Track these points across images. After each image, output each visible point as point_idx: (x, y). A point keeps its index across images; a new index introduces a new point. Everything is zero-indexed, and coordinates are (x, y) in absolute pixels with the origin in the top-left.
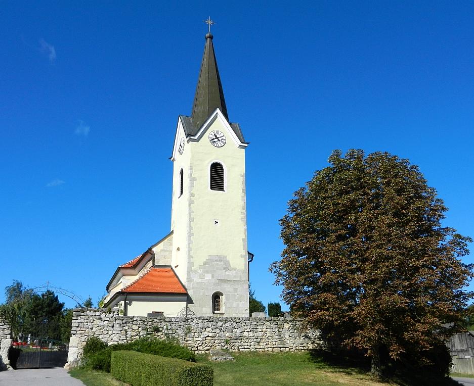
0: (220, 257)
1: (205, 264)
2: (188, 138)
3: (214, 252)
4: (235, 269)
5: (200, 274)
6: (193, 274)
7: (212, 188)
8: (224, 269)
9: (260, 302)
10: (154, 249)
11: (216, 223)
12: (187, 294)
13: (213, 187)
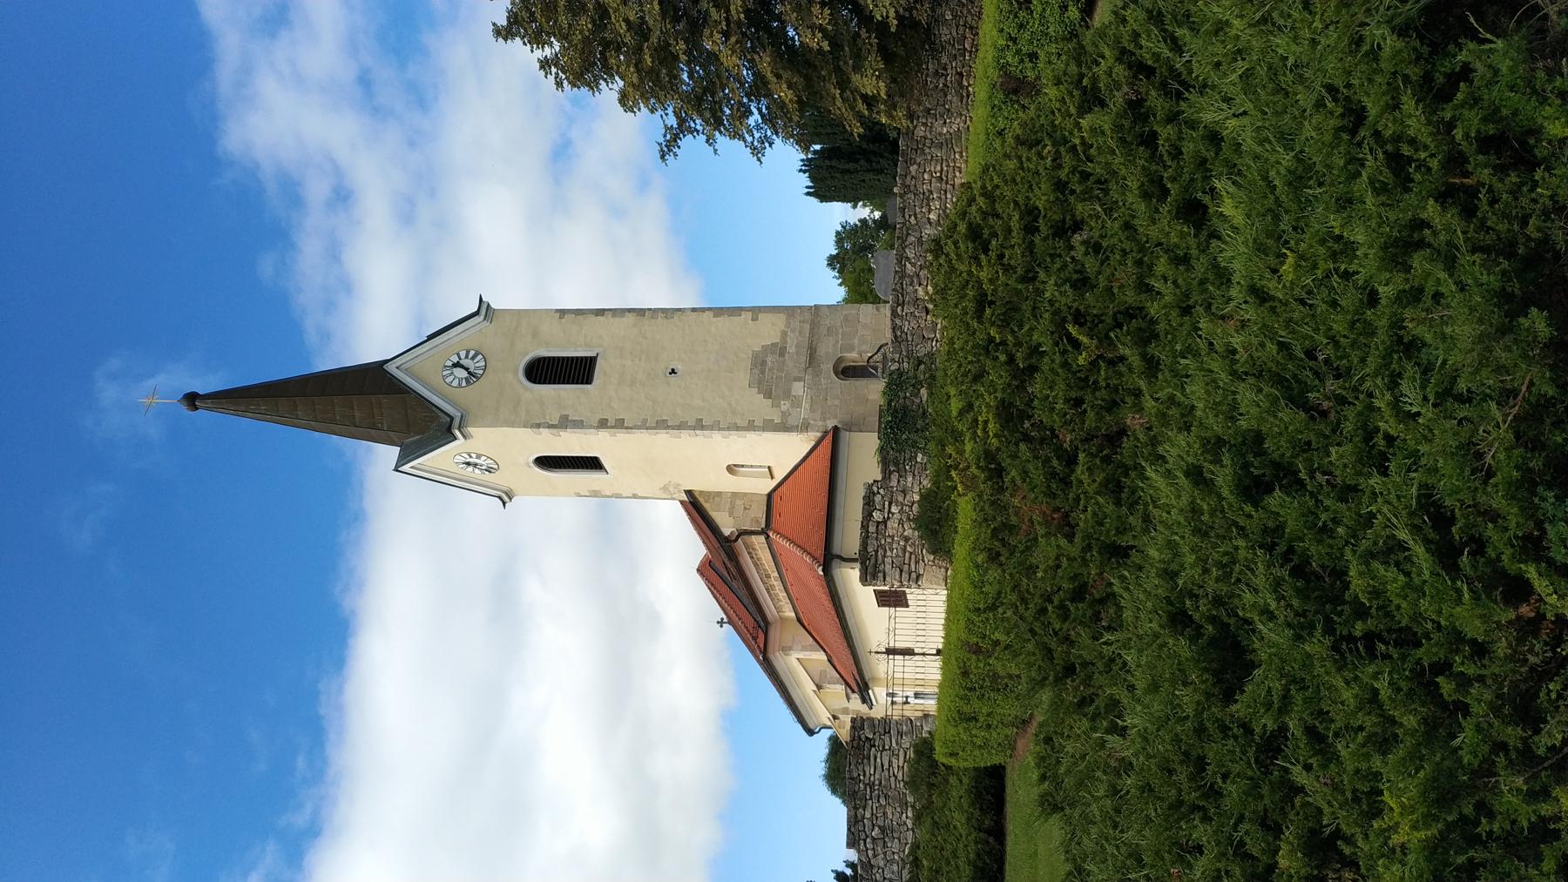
0: (754, 365)
1: (768, 395)
2: (457, 433)
3: (743, 376)
4: (784, 334)
5: (792, 406)
6: (791, 421)
7: (589, 381)
8: (782, 354)
9: (834, 791)
10: (727, 532)
11: (673, 372)
12: (836, 429)
13: (587, 379)
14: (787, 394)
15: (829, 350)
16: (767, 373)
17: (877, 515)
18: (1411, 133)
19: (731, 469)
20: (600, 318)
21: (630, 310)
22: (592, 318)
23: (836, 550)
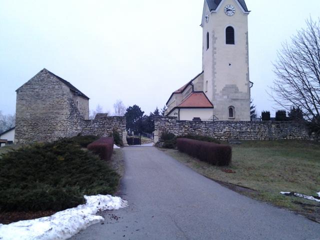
3: (228, 83)
4: (241, 92)
13: (227, 43)
14: (224, 95)
15: (236, 104)
16: (231, 89)
17: (170, 120)
18: (17, 192)
19: (207, 81)
20: (245, 44)
21: (248, 52)
22: (246, 41)
23: (181, 110)
